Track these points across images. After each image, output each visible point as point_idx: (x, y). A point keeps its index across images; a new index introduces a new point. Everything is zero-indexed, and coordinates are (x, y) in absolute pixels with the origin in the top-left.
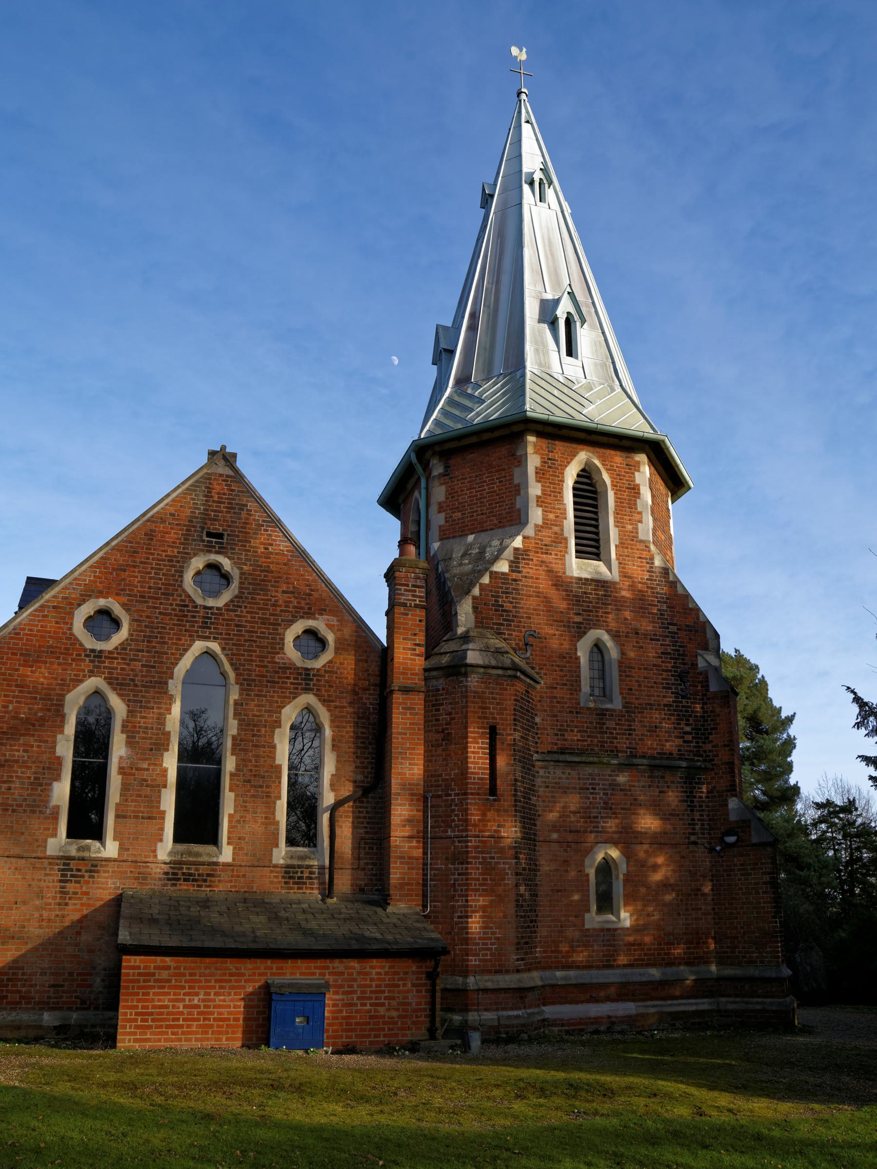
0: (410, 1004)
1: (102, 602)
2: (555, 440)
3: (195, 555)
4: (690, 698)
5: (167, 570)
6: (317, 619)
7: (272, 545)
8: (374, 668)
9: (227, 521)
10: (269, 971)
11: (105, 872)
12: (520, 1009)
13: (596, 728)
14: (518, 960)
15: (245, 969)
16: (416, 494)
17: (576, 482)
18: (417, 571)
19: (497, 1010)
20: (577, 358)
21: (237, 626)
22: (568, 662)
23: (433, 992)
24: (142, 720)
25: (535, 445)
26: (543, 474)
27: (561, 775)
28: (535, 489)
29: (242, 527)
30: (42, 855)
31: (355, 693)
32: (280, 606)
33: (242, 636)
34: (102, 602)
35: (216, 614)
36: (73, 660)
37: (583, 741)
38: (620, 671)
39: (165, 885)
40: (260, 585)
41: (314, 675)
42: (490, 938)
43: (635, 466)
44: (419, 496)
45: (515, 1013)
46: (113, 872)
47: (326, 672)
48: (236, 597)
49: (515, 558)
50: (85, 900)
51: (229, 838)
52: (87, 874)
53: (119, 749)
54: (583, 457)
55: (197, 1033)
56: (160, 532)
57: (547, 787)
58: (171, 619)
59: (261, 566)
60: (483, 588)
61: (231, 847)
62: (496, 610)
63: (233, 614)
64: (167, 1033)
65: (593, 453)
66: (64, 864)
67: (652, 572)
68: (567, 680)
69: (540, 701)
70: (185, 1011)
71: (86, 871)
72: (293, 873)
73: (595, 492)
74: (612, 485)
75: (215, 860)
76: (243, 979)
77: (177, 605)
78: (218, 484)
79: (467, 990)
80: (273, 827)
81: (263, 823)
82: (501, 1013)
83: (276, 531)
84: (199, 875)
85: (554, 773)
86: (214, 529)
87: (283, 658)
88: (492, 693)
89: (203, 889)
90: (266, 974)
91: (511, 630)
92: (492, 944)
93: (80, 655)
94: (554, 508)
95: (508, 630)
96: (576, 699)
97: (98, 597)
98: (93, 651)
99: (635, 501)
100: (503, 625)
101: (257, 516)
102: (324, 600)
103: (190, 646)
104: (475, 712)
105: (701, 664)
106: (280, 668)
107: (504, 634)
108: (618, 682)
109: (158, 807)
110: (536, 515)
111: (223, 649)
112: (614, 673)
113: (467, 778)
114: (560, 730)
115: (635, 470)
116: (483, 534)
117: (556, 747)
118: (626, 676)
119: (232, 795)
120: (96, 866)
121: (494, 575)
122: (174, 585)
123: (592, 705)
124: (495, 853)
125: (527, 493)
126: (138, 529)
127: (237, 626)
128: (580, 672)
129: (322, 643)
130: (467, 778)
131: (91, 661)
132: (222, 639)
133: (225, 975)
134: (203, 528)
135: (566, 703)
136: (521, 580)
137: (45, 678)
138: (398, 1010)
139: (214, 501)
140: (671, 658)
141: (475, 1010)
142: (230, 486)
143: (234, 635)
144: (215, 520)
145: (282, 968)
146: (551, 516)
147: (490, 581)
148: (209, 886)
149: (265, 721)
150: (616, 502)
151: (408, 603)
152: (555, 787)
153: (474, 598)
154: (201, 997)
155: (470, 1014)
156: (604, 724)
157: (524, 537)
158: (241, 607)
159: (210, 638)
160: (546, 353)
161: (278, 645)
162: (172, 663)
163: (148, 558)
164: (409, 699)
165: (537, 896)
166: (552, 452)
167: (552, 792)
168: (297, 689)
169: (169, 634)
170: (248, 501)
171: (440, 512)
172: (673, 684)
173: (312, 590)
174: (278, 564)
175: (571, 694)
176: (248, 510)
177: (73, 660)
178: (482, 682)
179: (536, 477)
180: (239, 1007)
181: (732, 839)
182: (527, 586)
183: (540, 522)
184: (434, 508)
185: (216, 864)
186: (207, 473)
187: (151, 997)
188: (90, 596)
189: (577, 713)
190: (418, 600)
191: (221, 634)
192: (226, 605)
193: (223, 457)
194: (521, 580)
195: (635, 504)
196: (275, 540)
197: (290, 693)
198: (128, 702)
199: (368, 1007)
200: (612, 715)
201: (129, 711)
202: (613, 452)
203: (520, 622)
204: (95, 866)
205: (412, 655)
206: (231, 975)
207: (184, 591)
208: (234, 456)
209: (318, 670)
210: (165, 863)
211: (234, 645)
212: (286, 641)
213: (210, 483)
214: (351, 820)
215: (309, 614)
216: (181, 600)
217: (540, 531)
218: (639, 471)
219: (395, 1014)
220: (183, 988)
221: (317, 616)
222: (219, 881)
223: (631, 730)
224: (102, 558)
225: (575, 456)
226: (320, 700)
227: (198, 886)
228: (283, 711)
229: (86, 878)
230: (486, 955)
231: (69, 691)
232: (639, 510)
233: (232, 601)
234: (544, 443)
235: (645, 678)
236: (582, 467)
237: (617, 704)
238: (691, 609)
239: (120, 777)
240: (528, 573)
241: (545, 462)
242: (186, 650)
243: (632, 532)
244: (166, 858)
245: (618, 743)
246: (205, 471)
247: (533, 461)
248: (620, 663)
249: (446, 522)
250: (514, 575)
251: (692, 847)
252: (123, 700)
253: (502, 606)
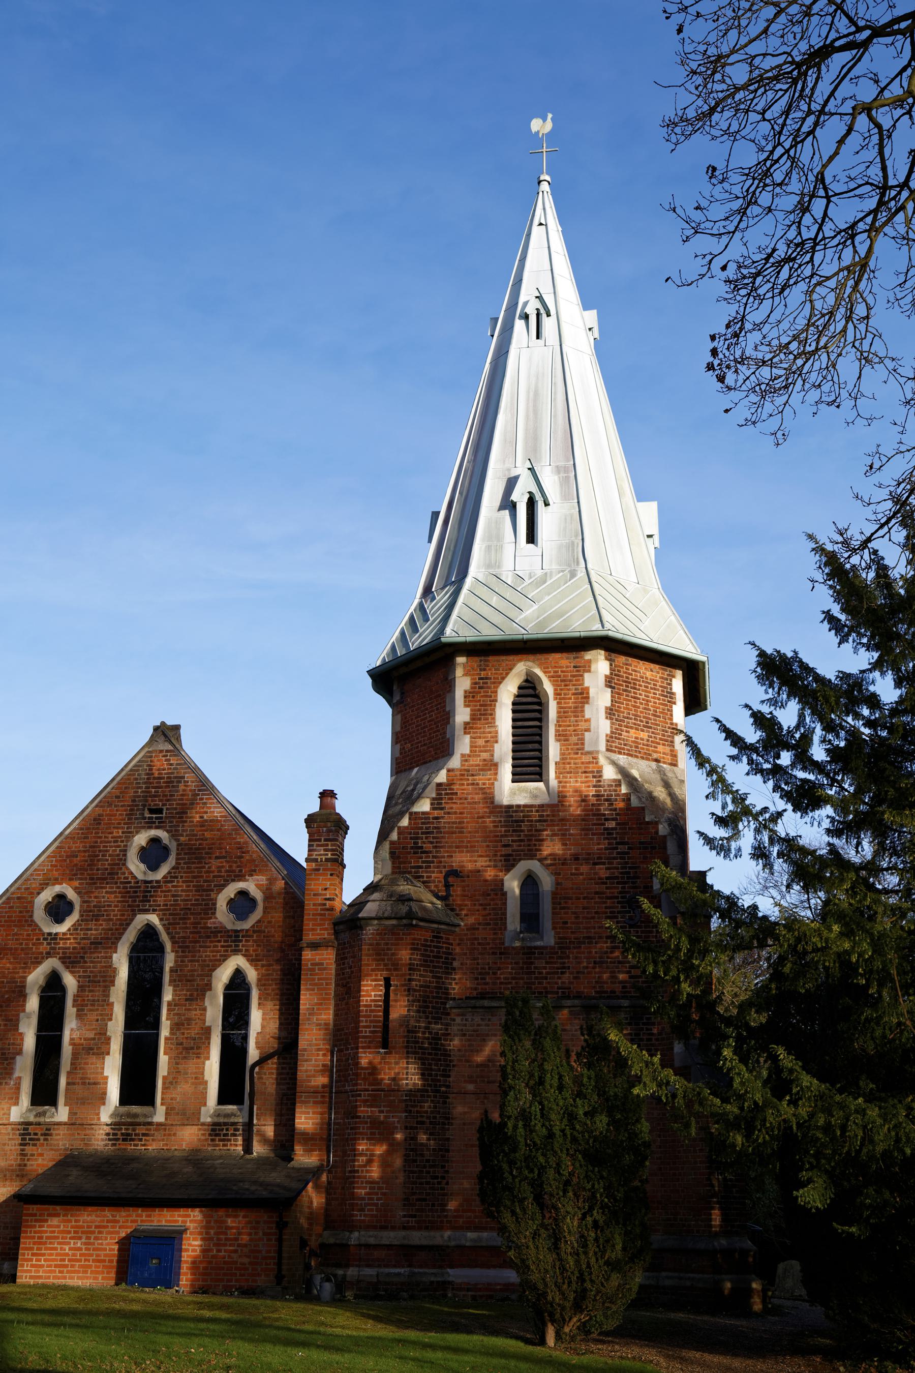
0: (260, 1252)
1: (57, 889)
2: (488, 655)
3: (137, 833)
4: (640, 927)
5: (113, 851)
6: (247, 880)
7: (206, 813)
9: (166, 796)
10: (139, 1219)
11: (57, 1135)
12: (403, 1267)
13: (522, 968)
14: (404, 1216)
15: (120, 1216)
18: (329, 824)
19: (379, 1266)
20: (537, 546)
21: (173, 896)
22: (493, 900)
23: (280, 1240)
24: (90, 994)
25: (464, 665)
26: (473, 697)
27: (480, 1022)
28: (462, 715)
29: (179, 800)
30: (6, 1122)
31: (283, 951)
32: (213, 872)
33: (179, 905)
34: (57, 889)
35: (155, 887)
36: (33, 944)
37: (506, 983)
38: (553, 903)
39: (106, 1145)
40: (194, 853)
41: (243, 936)
42: (377, 1194)
43: (585, 666)
45: (397, 1270)
46: (64, 1134)
47: (254, 932)
48: (173, 868)
49: (438, 794)
51: (162, 1099)
52: (42, 1138)
54: (520, 669)
55: (78, 1272)
56: (107, 815)
57: (464, 1035)
58: (116, 897)
59: (196, 835)
61: (164, 1108)
62: (415, 853)
63: (170, 885)
64: (55, 1271)
65: (533, 662)
66: (24, 1129)
67: (600, 786)
68: (490, 919)
69: (459, 944)
70: (70, 1253)
71: (42, 1135)
72: (219, 1130)
73: (540, 704)
74: (555, 694)
75: (150, 1120)
76: (118, 1225)
77: (121, 883)
78: (158, 761)
79: (349, 1246)
80: (202, 1087)
81: (193, 1084)
82: (382, 1270)
83: (210, 799)
84: (136, 1135)
85: (472, 1020)
86: (155, 805)
87: (214, 923)
88: (387, 944)
89: (139, 1148)
90: (136, 1221)
91: (430, 872)
92: (378, 1199)
93: (39, 939)
94: (484, 733)
95: (427, 872)
96: (500, 939)
97: (54, 884)
98: (50, 934)
99: (583, 707)
100: (421, 867)
102: (254, 861)
103: (132, 920)
104: (368, 965)
106: (211, 932)
107: (423, 877)
108: (550, 915)
109: (103, 1073)
110: (463, 745)
111: (161, 920)
112: (546, 906)
113: (358, 1032)
114: (480, 974)
115: (585, 671)
117: (475, 992)
118: (562, 908)
119: (166, 1057)
120: (49, 1130)
121: (414, 816)
122: (118, 864)
124: (384, 1106)
125: (454, 721)
127: (173, 896)
128: (506, 909)
130: (358, 1032)
131: (49, 944)
132: (160, 910)
133: (103, 1221)
134: (144, 806)
135: (489, 944)
136: (443, 818)
137: (10, 963)
138: (249, 1257)
139: (154, 778)
140: (618, 883)
141: (357, 1266)
142: (169, 760)
143: (171, 905)
144: (155, 796)
145: (150, 1216)
147: (410, 823)
148: (144, 1145)
149: (198, 985)
150: (558, 712)
151: (319, 858)
152: (472, 1035)
153: (392, 843)
154: (83, 1240)
155: (351, 1269)
156: (532, 963)
157: (449, 771)
158: (177, 877)
159: (149, 910)
160: (500, 548)
161: (211, 908)
162: (116, 939)
163: (96, 842)
164: (317, 954)
165: (448, 1151)
166: (485, 670)
167: (469, 1040)
168: (227, 951)
169: (114, 911)
170: (185, 773)
172: (619, 912)
173: (243, 853)
174: (212, 830)
175: (494, 934)
176: (185, 782)
177: (33, 944)
178: (377, 934)
179: (465, 702)
180: (114, 1250)
182: (449, 823)
185: (151, 1124)
186: (148, 752)
187: (44, 1240)
188: (47, 884)
189: (501, 953)
190: (329, 854)
191: (159, 905)
192: (164, 877)
193: (167, 734)
194: (443, 818)
195: (583, 711)
196: (210, 808)
197: (221, 956)
199: (223, 1253)
200: (542, 953)
201: (79, 987)
202: (558, 655)
203: (441, 862)
204: (48, 1130)
205: (322, 910)
206: (108, 1221)
207: (128, 869)
209: (247, 931)
210: (107, 1125)
211: (170, 914)
212: (218, 906)
213: (151, 761)
214: (274, 1076)
216: (125, 878)
217: (466, 761)
218: (589, 671)
219: (246, 1260)
220: (69, 1232)
221: (247, 877)
222: (153, 1140)
223: (564, 968)
224: (58, 847)
225: (511, 669)
226: (248, 960)
227: (135, 1145)
229: (42, 1141)
230: (372, 1210)
231: (30, 973)
232: (587, 717)
233: (169, 873)
234: (475, 661)
235: (584, 908)
236: (523, 678)
237: (549, 939)
239: (71, 1047)
240: (452, 808)
242: (128, 925)
243: (577, 744)
244: (109, 1121)
245: (549, 983)
246: (146, 749)
247: (462, 684)
248: (554, 894)
249: (401, 754)
250: (436, 813)
252: (74, 976)
253: (422, 847)
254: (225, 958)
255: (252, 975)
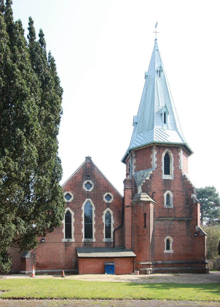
8: (121, 202)
16: (129, 160)
17: (165, 156)
44: (130, 161)
50: (70, 250)
53: (73, 220)
60: (144, 183)
73: (168, 157)
101: (97, 171)
105: (192, 197)
111: (92, 200)
116: (144, 170)
121: (146, 180)
123: (166, 207)
126: (73, 176)
129: (111, 197)
146: (159, 165)
153: (142, 186)
157: (153, 171)
171: (134, 165)
181: (196, 235)
183: (156, 167)
184: (133, 164)
185: (93, 242)
192: (92, 191)
193: (88, 159)
198: (74, 212)
204: (71, 243)
207: (83, 188)
208: (91, 158)
215: (108, 192)
228: (104, 212)
237: (172, 207)
238: (190, 184)
241: (158, 153)
242: (84, 201)
251: (187, 236)
252: (73, 212)
254: (106, 209)
255: (111, 212)
